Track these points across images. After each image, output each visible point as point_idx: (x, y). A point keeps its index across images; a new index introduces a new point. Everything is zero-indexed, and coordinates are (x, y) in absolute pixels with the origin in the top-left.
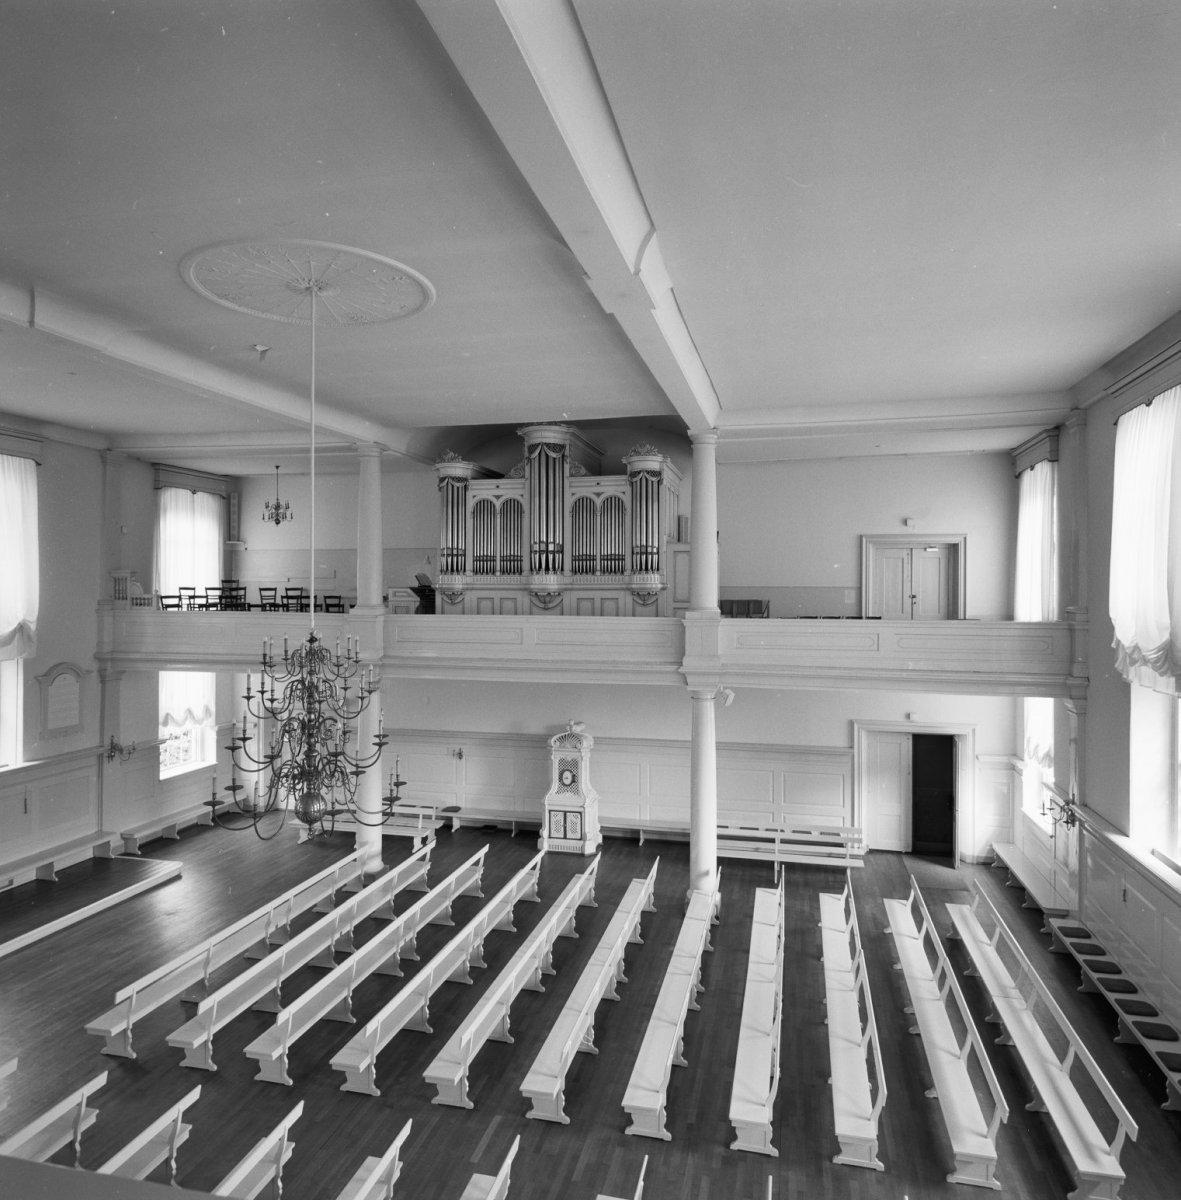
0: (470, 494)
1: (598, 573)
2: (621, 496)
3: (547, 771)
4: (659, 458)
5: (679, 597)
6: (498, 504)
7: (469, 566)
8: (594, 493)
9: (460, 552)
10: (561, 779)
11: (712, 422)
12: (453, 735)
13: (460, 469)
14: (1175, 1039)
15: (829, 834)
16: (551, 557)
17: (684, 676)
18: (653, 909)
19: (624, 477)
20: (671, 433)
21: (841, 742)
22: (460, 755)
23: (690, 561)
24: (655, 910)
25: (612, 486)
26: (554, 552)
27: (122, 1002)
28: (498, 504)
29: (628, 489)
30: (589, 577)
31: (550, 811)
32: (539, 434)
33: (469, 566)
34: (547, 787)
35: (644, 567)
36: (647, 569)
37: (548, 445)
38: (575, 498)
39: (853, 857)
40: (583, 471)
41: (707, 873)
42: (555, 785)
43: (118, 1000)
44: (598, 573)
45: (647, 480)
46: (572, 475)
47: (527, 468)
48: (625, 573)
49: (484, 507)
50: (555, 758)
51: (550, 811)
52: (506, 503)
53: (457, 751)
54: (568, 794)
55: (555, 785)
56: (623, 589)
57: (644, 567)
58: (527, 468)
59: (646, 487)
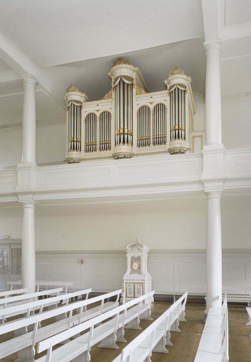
1: (152, 145)
3: (126, 262)
5: (199, 139)
7: (83, 148)
8: (150, 103)
9: (78, 140)
12: (78, 252)
16: (126, 136)
18: (184, 320)
19: (166, 91)
22: (82, 262)
23: (205, 133)
24: (186, 321)
25: (161, 97)
26: (128, 134)
29: (168, 98)
30: (147, 147)
31: (126, 283)
32: (119, 71)
33: (83, 148)
34: (125, 271)
35: (177, 137)
37: (124, 77)
38: (139, 107)
40: (143, 91)
41: (217, 298)
42: (129, 270)
44: (152, 145)
45: (178, 89)
46: (137, 94)
47: (113, 94)
48: (167, 143)
49: (91, 117)
50: (129, 256)
51: (126, 283)
53: (80, 260)
54: (136, 275)
55: (129, 270)
57: (177, 137)
58: (113, 94)
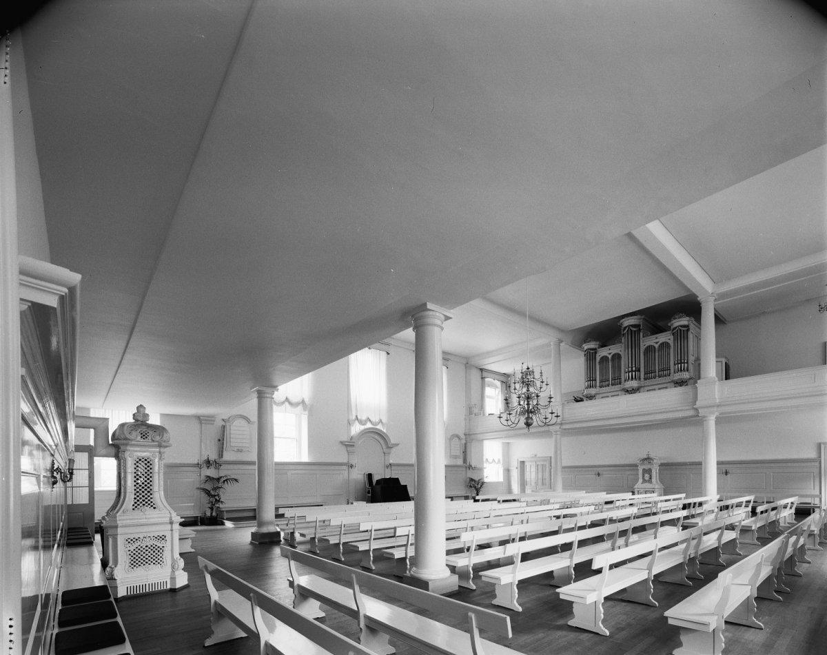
0: (597, 355)
2: (668, 341)
4: (688, 318)
6: (610, 357)
7: (598, 384)
10: (643, 477)
11: (710, 291)
13: (592, 345)
14: (447, 357)
15: (644, 415)
16: (634, 373)
17: (696, 409)
19: (670, 332)
20: (690, 307)
21: (812, 454)
27: (714, 530)
28: (610, 357)
34: (637, 480)
36: (681, 370)
37: (632, 326)
39: (739, 505)
42: (641, 480)
43: (356, 609)
49: (604, 359)
52: (614, 356)
56: (669, 382)
59: (681, 334)
